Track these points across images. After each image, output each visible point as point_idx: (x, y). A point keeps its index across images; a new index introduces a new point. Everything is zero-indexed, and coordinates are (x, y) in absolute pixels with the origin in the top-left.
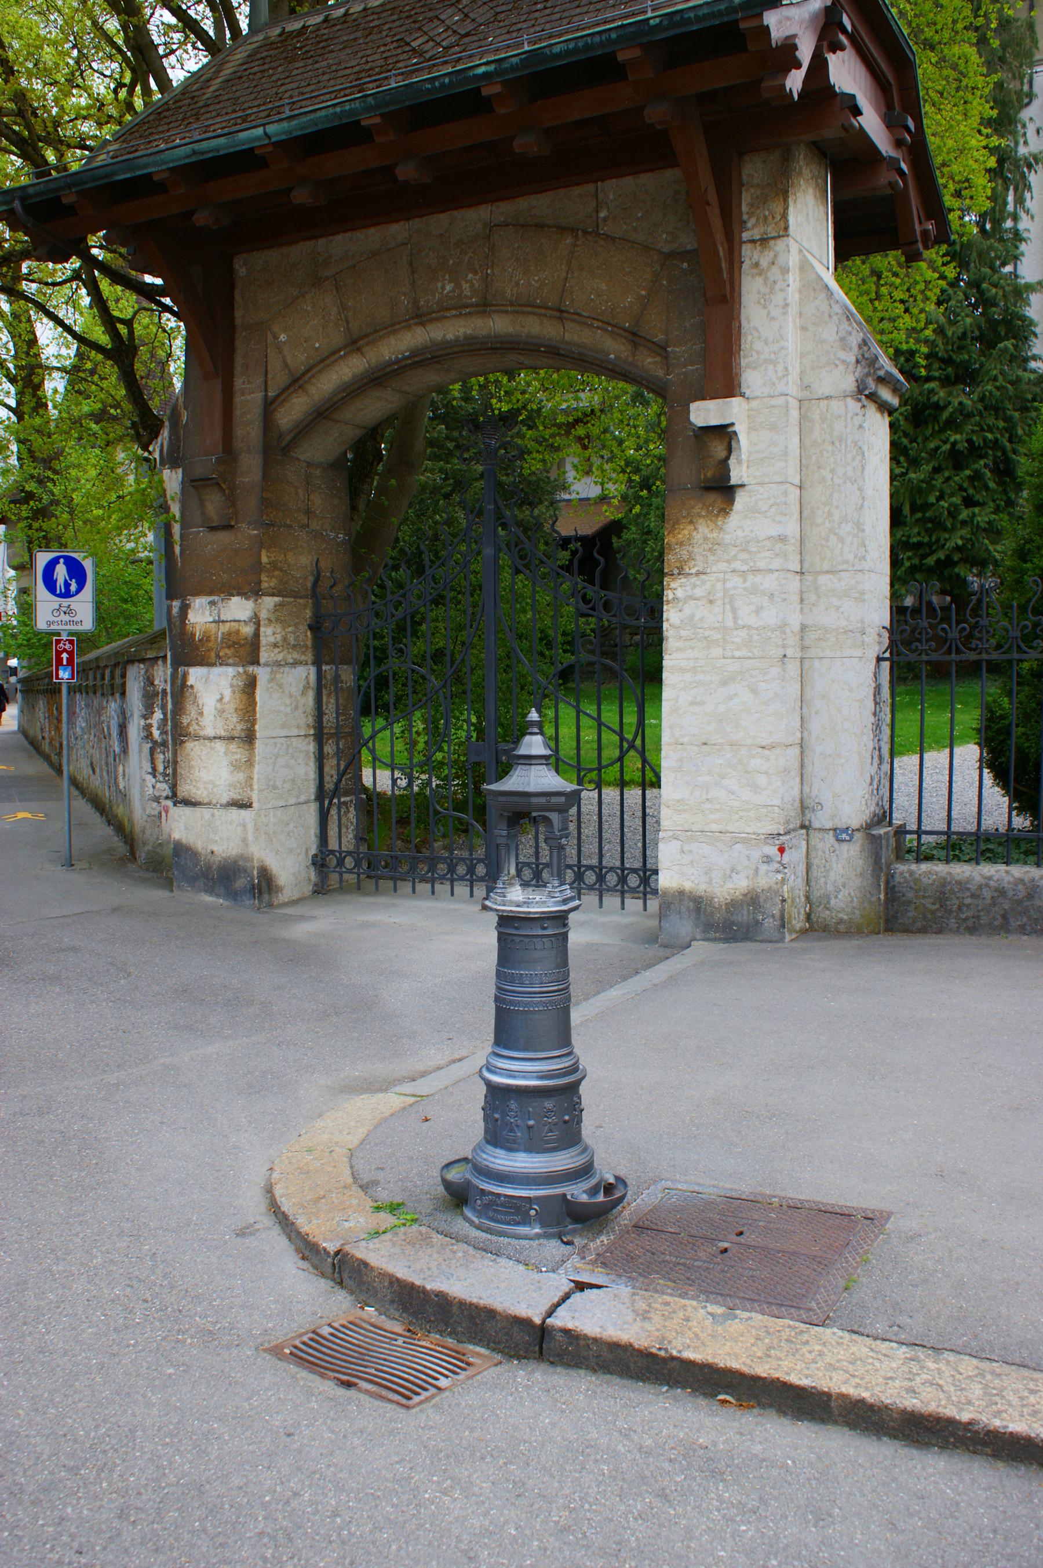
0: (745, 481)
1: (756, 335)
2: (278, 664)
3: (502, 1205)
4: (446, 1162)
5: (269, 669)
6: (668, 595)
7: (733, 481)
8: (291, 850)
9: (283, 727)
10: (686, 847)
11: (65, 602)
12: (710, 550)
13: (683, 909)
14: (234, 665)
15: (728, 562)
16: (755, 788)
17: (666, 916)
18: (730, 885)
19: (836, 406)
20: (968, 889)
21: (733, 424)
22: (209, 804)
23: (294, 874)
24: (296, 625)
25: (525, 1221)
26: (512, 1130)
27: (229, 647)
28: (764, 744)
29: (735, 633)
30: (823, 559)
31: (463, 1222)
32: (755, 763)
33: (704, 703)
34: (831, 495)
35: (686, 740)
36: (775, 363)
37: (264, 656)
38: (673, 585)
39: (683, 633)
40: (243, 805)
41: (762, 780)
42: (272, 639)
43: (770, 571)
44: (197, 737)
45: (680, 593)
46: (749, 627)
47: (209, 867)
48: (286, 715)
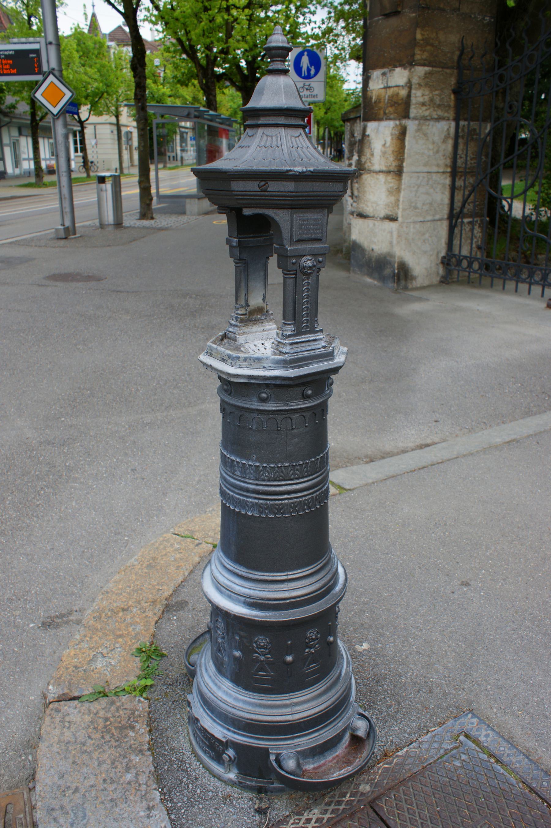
2: (425, 118)
5: (417, 122)
8: (425, 252)
9: (425, 165)
11: (307, 82)
14: (394, 119)
22: (373, 217)
23: (426, 269)
24: (442, 90)
27: (391, 106)
37: (413, 112)
40: (392, 219)
42: (421, 100)
44: (370, 171)
47: (370, 259)
48: (429, 156)
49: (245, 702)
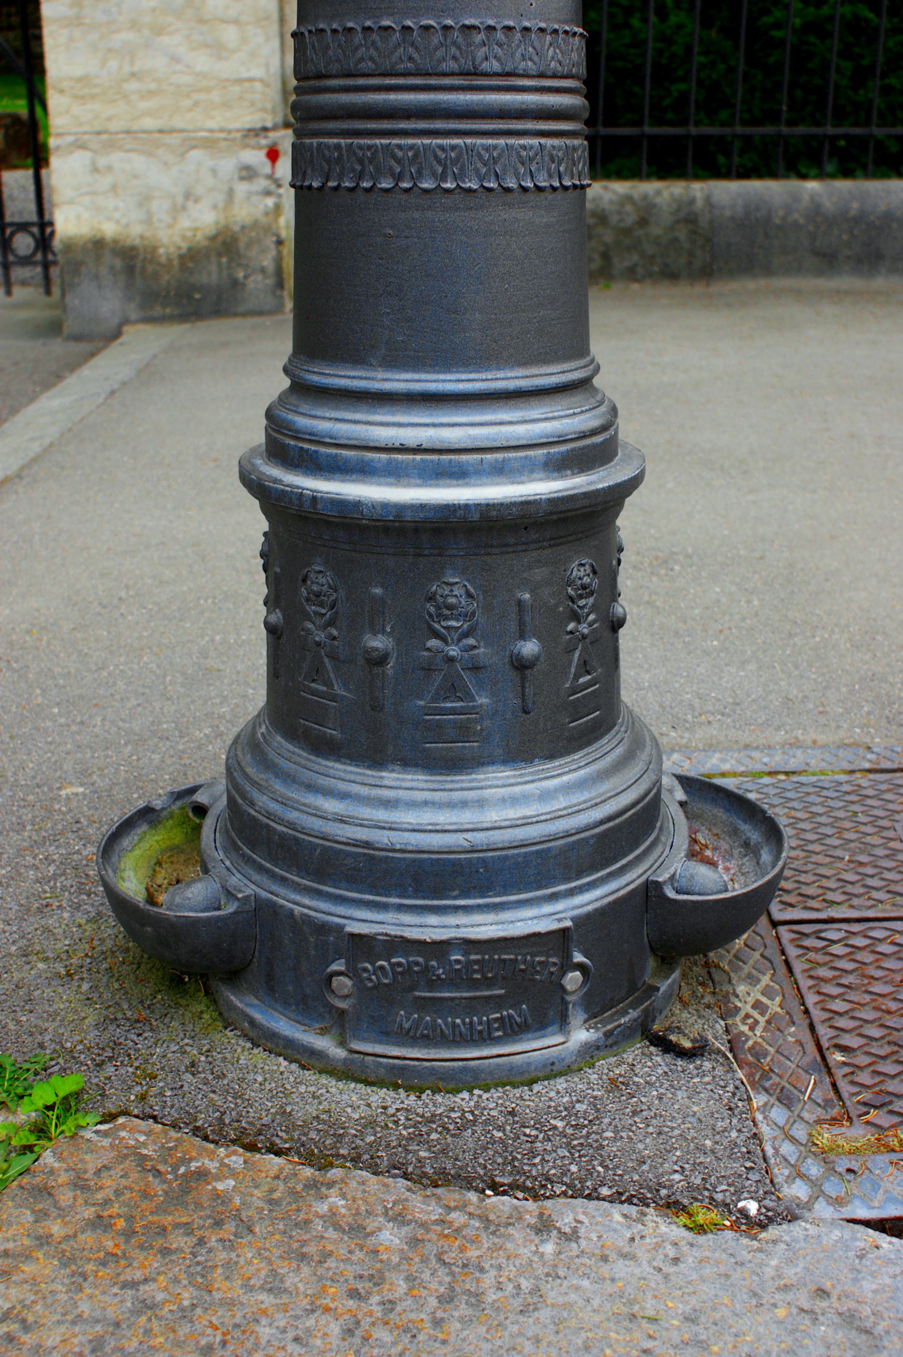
3: (457, 979)
4: (107, 829)
10: (102, 161)
13: (104, 271)
16: (219, 50)
18: (185, 223)
25: (549, 1012)
26: (454, 689)
41: (230, 35)
49: (567, 789)
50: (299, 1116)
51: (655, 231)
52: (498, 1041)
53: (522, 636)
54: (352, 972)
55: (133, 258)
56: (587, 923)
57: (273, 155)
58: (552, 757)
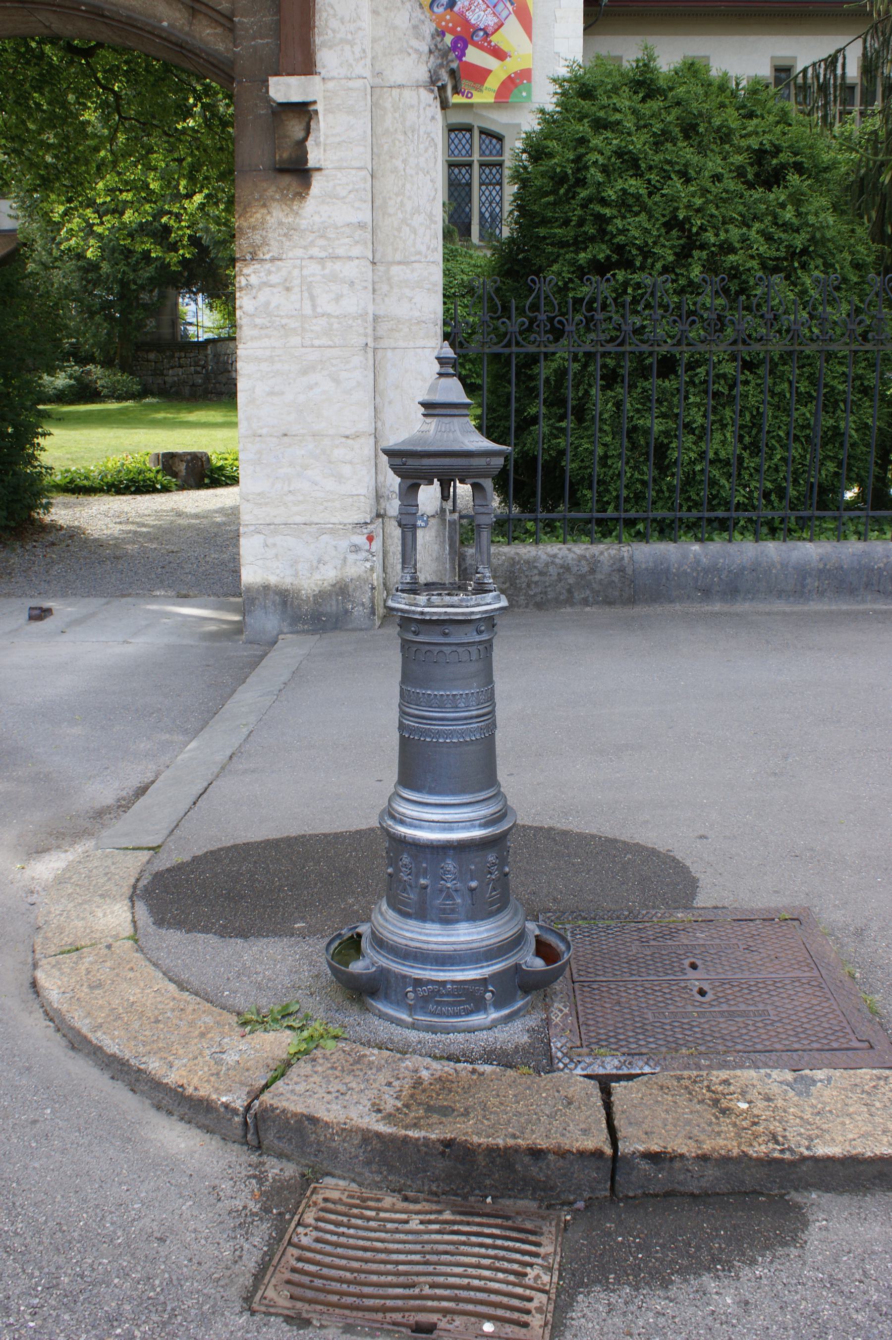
0: (323, 164)
1: (331, 12)
6: (241, 281)
7: (311, 164)
10: (270, 541)
12: (285, 235)
13: (269, 603)
15: (305, 248)
16: (340, 478)
17: (250, 611)
18: (317, 576)
19: (409, 96)
20: (536, 567)
21: (315, 102)
25: (479, 1006)
26: (449, 897)
28: (348, 433)
29: (314, 321)
30: (396, 250)
31: (376, 1021)
32: (339, 453)
33: (283, 393)
34: (404, 185)
35: (264, 431)
36: (352, 43)
38: (246, 271)
39: (258, 321)
41: (347, 470)
43: (350, 258)
45: (253, 280)
46: (329, 315)
50: (396, 1040)
51: (599, 576)
52: (461, 1016)
53: (472, 880)
54: (414, 991)
55: (286, 596)
56: (493, 976)
57: (370, 539)
58: (482, 919)
